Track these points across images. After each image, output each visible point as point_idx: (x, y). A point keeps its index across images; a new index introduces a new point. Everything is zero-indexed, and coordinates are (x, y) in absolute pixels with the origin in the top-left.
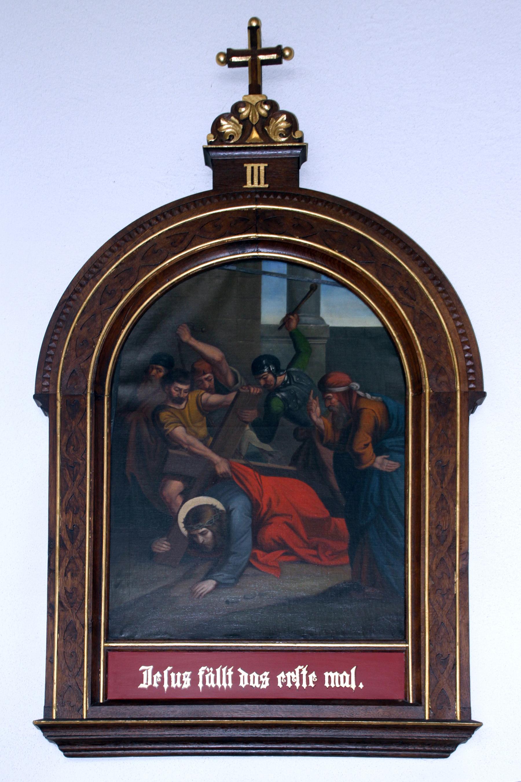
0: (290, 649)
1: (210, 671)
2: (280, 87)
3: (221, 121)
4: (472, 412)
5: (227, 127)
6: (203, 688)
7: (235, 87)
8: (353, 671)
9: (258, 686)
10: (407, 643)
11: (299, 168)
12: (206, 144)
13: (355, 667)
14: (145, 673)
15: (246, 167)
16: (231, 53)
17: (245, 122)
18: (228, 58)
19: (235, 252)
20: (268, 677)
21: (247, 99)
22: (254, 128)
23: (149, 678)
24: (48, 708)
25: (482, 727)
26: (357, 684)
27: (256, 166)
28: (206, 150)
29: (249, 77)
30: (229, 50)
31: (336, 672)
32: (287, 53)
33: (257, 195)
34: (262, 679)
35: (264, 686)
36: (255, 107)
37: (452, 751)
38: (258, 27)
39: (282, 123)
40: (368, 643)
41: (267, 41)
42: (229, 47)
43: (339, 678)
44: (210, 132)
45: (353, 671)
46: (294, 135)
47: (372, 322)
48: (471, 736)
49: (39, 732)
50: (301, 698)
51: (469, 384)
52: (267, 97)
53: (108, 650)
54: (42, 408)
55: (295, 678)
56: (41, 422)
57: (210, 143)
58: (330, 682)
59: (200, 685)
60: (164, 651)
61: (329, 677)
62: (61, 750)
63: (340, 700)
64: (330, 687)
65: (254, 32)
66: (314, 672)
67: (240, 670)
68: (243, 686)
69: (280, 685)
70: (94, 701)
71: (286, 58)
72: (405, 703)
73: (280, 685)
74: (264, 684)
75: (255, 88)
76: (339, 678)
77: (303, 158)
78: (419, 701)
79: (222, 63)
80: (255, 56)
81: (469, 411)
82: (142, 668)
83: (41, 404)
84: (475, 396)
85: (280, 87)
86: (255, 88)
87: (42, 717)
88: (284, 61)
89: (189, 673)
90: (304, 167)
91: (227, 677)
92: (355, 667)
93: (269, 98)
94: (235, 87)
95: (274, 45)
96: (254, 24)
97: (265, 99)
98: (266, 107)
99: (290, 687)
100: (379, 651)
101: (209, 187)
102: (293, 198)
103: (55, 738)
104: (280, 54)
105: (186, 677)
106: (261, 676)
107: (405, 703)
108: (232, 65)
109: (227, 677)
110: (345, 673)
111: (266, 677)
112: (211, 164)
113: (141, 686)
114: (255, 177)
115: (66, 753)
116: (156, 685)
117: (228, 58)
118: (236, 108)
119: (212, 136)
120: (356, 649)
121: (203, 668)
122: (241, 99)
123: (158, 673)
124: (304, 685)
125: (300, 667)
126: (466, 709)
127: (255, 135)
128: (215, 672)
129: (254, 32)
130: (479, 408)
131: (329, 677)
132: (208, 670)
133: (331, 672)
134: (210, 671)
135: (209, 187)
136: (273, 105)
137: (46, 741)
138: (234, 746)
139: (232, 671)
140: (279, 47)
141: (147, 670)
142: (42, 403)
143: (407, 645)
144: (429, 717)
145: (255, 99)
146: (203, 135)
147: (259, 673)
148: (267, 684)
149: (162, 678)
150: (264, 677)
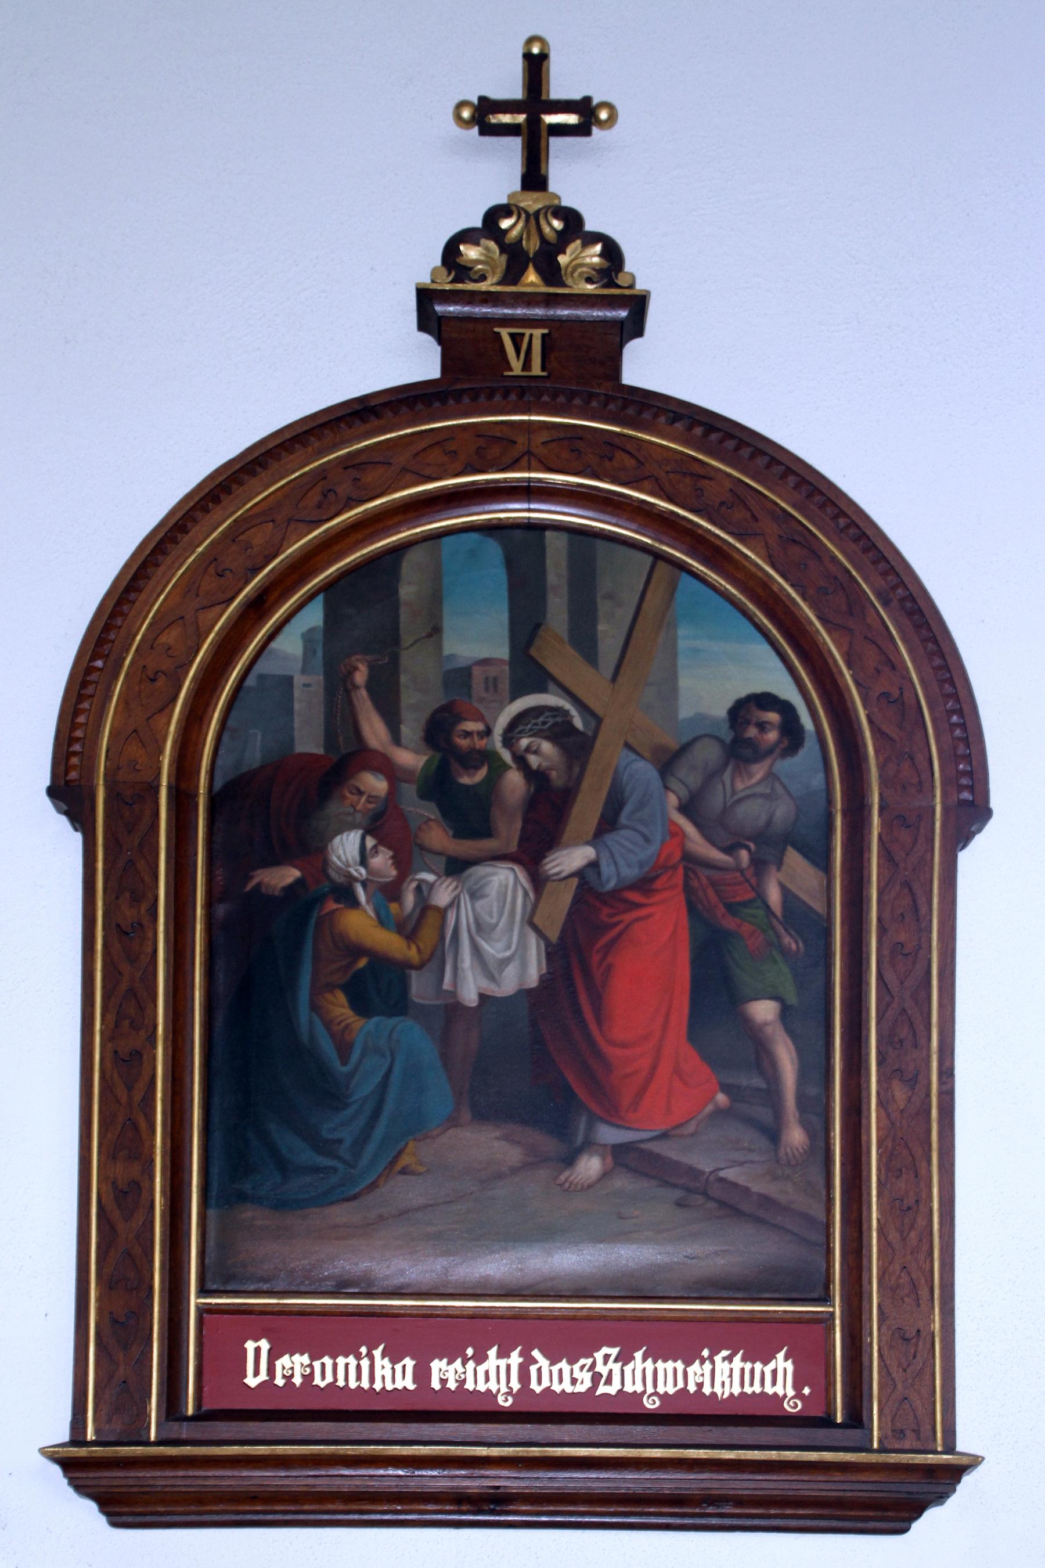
2: (577, 177)
3: (462, 248)
5: (471, 253)
7: (492, 174)
9: (569, 1389)
12: (425, 279)
13: (519, 1348)
22: (531, 255)
23: (267, 1367)
25: (980, 1469)
26: (798, 1386)
27: (531, 329)
28: (425, 297)
30: (482, 99)
31: (679, 1362)
32: (603, 115)
33: (526, 393)
34: (577, 1374)
35: (580, 1388)
36: (533, 219)
38: (544, 57)
43: (763, 1374)
47: (314, 616)
48: (955, 1491)
49: (56, 1470)
50: (697, 1412)
51: (959, 792)
52: (559, 198)
53: (202, 1311)
54: (66, 813)
55: (383, 1367)
57: (433, 281)
63: (725, 1416)
65: (535, 66)
66: (564, 1360)
67: (536, 1353)
68: (538, 1389)
69: (436, 1385)
71: (601, 124)
73: (436, 1385)
74: (582, 1383)
75: (534, 177)
76: (763, 1374)
77: (635, 326)
78: (857, 1418)
80: (532, 116)
81: (957, 845)
83: (65, 808)
84: (971, 811)
85: (577, 177)
86: (534, 177)
87: (66, 1438)
93: (566, 202)
94: (492, 174)
95: (577, 95)
96: (536, 50)
98: (557, 224)
99: (453, 1389)
102: (542, 395)
103: (90, 1490)
104: (588, 115)
105: (584, 1366)
106: (576, 1367)
107: (827, 1421)
108: (488, 130)
112: (436, 334)
116: (280, 1382)
117: (483, 115)
118: (493, 215)
119: (444, 271)
120: (628, 1314)
122: (503, 200)
125: (605, 1350)
126: (950, 1447)
127: (532, 277)
129: (535, 66)
136: (572, 219)
137: (70, 1491)
140: (587, 100)
142: (67, 805)
144: (156, 1437)
145: (532, 202)
146: (424, 264)
147: (572, 1362)
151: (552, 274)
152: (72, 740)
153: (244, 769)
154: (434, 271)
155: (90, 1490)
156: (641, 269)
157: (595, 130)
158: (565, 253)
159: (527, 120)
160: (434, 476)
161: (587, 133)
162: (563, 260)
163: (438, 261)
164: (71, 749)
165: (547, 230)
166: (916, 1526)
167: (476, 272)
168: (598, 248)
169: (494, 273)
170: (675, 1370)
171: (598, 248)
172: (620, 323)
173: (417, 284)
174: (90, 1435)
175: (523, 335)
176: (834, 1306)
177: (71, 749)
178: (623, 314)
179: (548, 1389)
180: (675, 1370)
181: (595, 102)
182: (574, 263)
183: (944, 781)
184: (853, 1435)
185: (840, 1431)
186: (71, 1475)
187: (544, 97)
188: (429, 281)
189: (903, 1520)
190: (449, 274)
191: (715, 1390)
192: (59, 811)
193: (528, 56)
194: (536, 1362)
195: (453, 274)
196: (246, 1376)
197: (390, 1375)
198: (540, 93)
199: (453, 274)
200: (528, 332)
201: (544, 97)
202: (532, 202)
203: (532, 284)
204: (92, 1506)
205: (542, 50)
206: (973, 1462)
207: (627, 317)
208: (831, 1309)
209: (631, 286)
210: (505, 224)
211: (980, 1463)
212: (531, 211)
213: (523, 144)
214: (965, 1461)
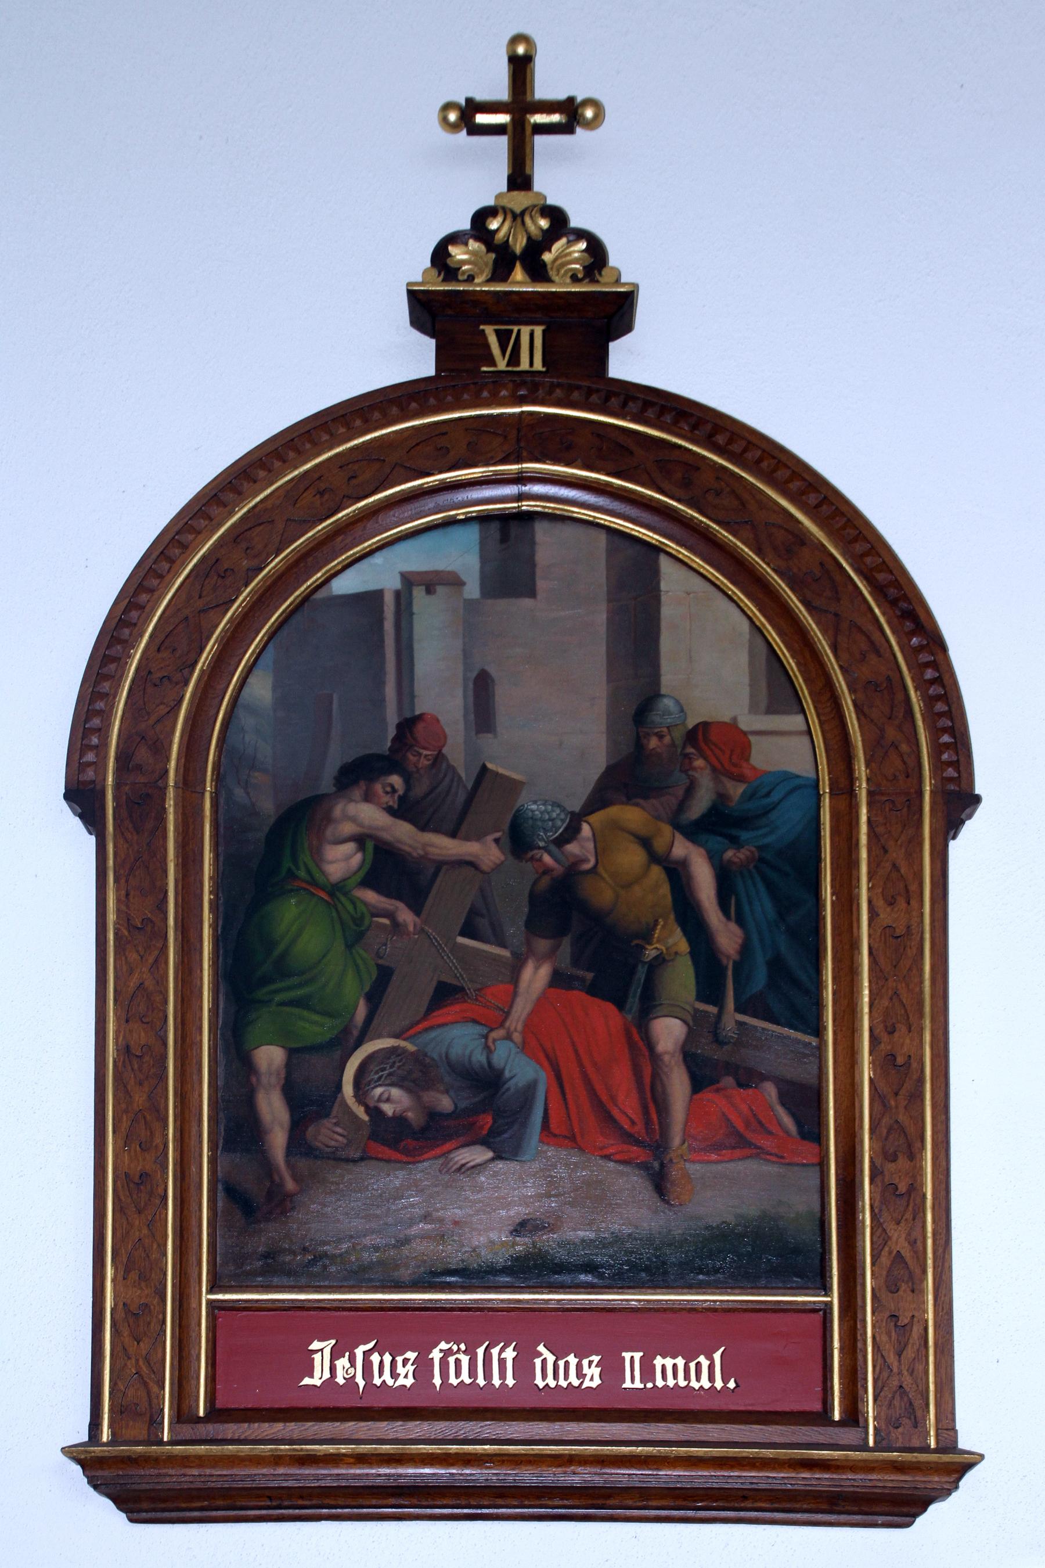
0: (335, 1305)
1: (459, 1349)
2: (561, 174)
3: (450, 248)
4: (954, 838)
5: (458, 253)
7: (480, 175)
8: (717, 1356)
10: (826, 1290)
14: (317, 1357)
15: (483, 331)
16: (471, 108)
18: (466, 116)
19: (192, 1188)
21: (504, 202)
23: (326, 1366)
26: (725, 1380)
27: (522, 321)
30: (469, 101)
32: (589, 113)
33: (528, 387)
36: (517, 217)
41: (548, 84)
42: (470, 95)
44: (429, 264)
46: (600, 274)
49: (78, 1469)
54: (82, 816)
56: (82, 845)
59: (437, 1381)
60: (775, 1311)
61: (664, 1367)
64: (666, 1386)
65: (521, 67)
70: (183, 1414)
75: (520, 178)
78: (853, 1416)
79: (454, 128)
80: (523, 114)
81: (948, 833)
82: (316, 1345)
84: (959, 802)
85: (561, 174)
86: (520, 178)
88: (579, 130)
89: (596, 1359)
91: (502, 1362)
93: (550, 201)
94: (480, 175)
95: (561, 95)
96: (521, 50)
98: (544, 223)
100: (775, 1311)
101: (429, 369)
104: (572, 115)
105: (590, 1363)
109: (502, 1362)
113: (307, 1381)
115: (135, 1515)
117: (466, 116)
118: (481, 217)
119: (435, 272)
121: (443, 1345)
122: (491, 202)
124: (496, 1382)
127: (519, 273)
128: (471, 1352)
129: (521, 67)
131: (664, 1367)
132: (455, 1348)
133: (668, 1358)
134: (459, 1349)
135: (429, 369)
136: (557, 217)
138: (390, 1510)
139: (514, 1350)
140: (571, 100)
141: (322, 1350)
144: (875, 1442)
145: (519, 201)
146: (416, 267)
150: (405, 1362)
151: (538, 272)
152: (83, 751)
154: (425, 272)
156: (626, 263)
157: (578, 130)
158: (550, 251)
159: (513, 120)
160: (161, 896)
162: (547, 257)
163: (428, 264)
164: (84, 760)
165: (532, 228)
166: (920, 1520)
167: (464, 272)
168: (583, 245)
169: (482, 272)
170: (675, 1366)
171: (583, 245)
175: (511, 331)
176: (832, 1297)
177: (84, 760)
180: (675, 1366)
181: (579, 99)
182: (559, 262)
183: (925, 772)
184: (849, 1435)
185: (837, 1430)
186: (94, 1473)
187: (529, 99)
189: (907, 1515)
190: (439, 275)
192: (75, 813)
194: (540, 1354)
197: (671, 1371)
198: (524, 93)
200: (516, 329)
201: (529, 99)
202: (519, 201)
205: (526, 51)
208: (829, 1299)
209: (618, 281)
210: (494, 225)
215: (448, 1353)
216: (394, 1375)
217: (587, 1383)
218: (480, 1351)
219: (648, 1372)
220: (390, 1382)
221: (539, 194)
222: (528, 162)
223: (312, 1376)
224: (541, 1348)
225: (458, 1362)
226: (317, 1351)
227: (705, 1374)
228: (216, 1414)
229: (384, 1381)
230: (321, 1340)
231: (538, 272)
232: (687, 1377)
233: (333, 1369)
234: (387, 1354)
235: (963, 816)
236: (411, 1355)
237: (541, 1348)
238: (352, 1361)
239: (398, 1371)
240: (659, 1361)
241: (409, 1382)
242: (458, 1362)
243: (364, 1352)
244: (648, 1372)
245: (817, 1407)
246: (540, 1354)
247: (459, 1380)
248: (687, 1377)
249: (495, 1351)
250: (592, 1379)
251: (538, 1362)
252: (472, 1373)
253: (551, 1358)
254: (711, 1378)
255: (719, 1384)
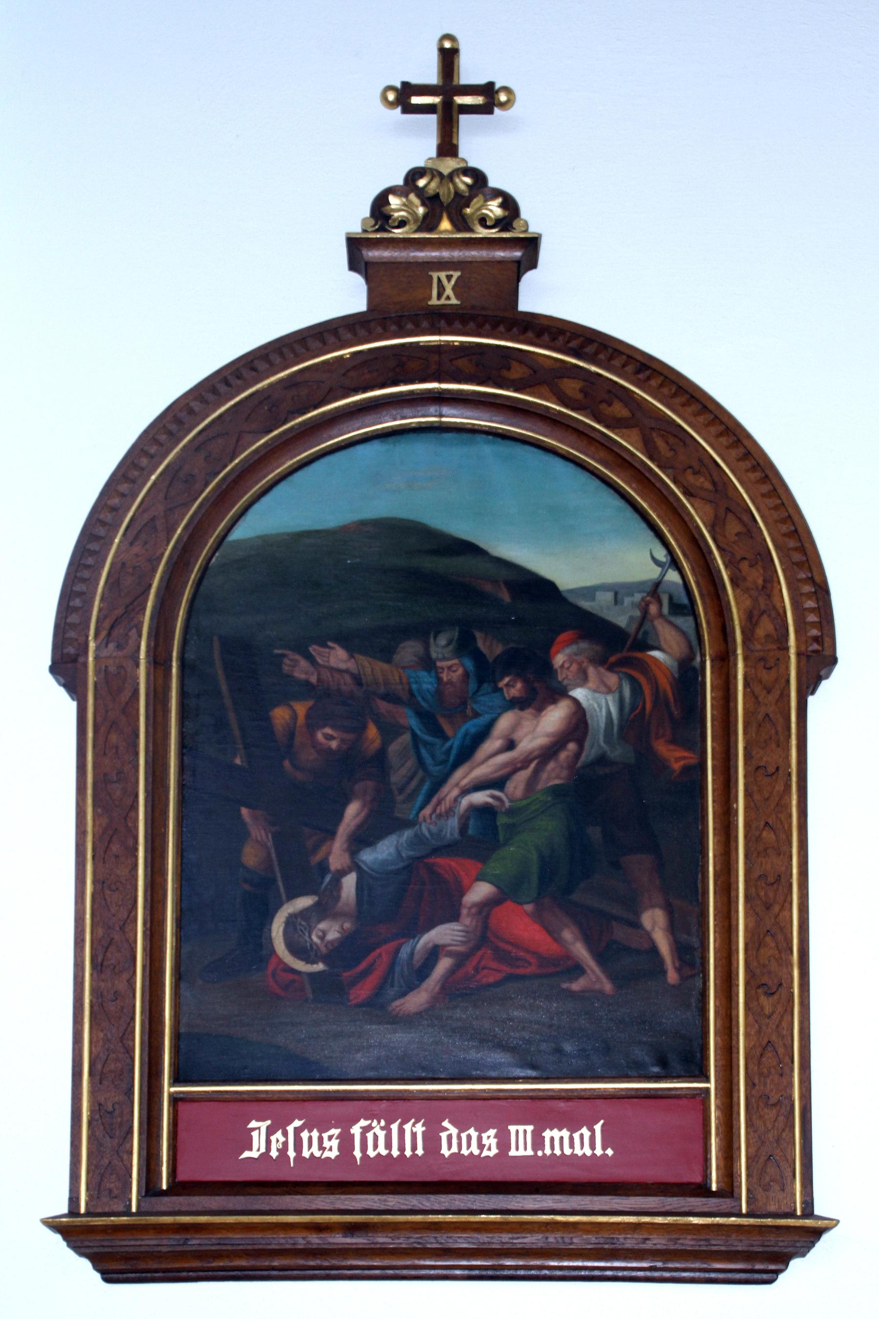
5: (394, 201)
6: (361, 1159)
7: (414, 144)
8: (598, 1127)
10: (707, 1080)
11: (518, 280)
12: (356, 228)
13: (602, 1122)
14: (255, 1134)
17: (431, 201)
18: (403, 97)
20: (495, 1137)
23: (262, 1141)
24: (74, 1200)
26: (604, 1148)
27: (445, 289)
28: (354, 244)
29: (438, 131)
30: (405, 85)
31: (565, 1130)
32: (503, 98)
37: (782, 1271)
39: (494, 209)
40: (145, 908)
41: (470, 73)
45: (598, 1127)
49: (58, 1237)
52: (467, 162)
56: (66, 707)
57: (365, 231)
58: (552, 1147)
59: (357, 1153)
62: (98, 1270)
65: (449, 58)
70: (150, 1188)
71: (502, 105)
72: (702, 1190)
75: (448, 147)
78: (729, 1190)
79: (391, 105)
80: (450, 97)
82: (253, 1124)
83: (62, 681)
84: (820, 660)
86: (448, 147)
87: (65, 1210)
88: (496, 110)
90: (528, 280)
92: (602, 1122)
93: (472, 164)
94: (414, 144)
95: (481, 80)
96: (447, 45)
97: (462, 165)
98: (468, 180)
103: (88, 1251)
107: (702, 1190)
108: (409, 109)
109: (414, 1135)
110: (585, 1131)
111: (328, 1148)
113: (246, 1154)
114: (445, 291)
115: (105, 1276)
116: (274, 1154)
117: (403, 97)
118: (414, 175)
119: (373, 222)
123: (280, 1132)
124: (408, 1153)
127: (445, 225)
128: (387, 1129)
129: (449, 58)
130: (824, 685)
131: (552, 1139)
133: (556, 1130)
136: (479, 177)
137: (71, 1253)
139: (423, 1125)
140: (491, 84)
141: (259, 1128)
142: (63, 677)
143: (173, 1089)
145: (448, 166)
146: (355, 218)
147: (481, 1130)
148: (494, 1151)
149: (285, 1144)
150: (330, 1138)
153: (398, 833)
154: (364, 220)
155: (88, 1251)
156: (534, 218)
161: (490, 112)
163: (367, 214)
168: (500, 200)
170: (562, 1138)
172: (518, 262)
173: (347, 233)
174: (83, 1210)
178: (518, 254)
179: (573, 1130)
184: (725, 1204)
187: (455, 83)
188: (359, 230)
191: (416, 1152)
193: (442, 50)
195: (379, 223)
196: (423, 1132)
197: (560, 1141)
199: (379, 223)
201: (455, 83)
202: (448, 166)
203: (446, 231)
204: (85, 1264)
206: (830, 1225)
207: (522, 256)
209: (526, 231)
211: (836, 1225)
212: (446, 171)
213: (438, 118)
214: (820, 1223)
215: (369, 1128)
216: (321, 1148)
217: (485, 1153)
218: (395, 1127)
219: (538, 1142)
220: (317, 1154)
221: (464, 160)
222: (455, 135)
223: (251, 1149)
224: (446, 1124)
225: (376, 1137)
226: (254, 1129)
227: (580, 1144)
228: (178, 1187)
229: (312, 1154)
230: (257, 1120)
231: (461, 223)
232: (572, 1146)
233: (268, 1142)
234: (315, 1130)
235: (822, 673)
236: (335, 1132)
237: (446, 1124)
238: (285, 1134)
239: (324, 1145)
240: (547, 1134)
241: (334, 1154)
242: (376, 1137)
243: (295, 1128)
244: (538, 1142)
245: (698, 1179)
246: (446, 1129)
247: (376, 1152)
248: (572, 1146)
249: (408, 1127)
250: (489, 1149)
251: (444, 1135)
252: (388, 1146)
253: (454, 1131)
254: (593, 1146)
255: (599, 1152)
